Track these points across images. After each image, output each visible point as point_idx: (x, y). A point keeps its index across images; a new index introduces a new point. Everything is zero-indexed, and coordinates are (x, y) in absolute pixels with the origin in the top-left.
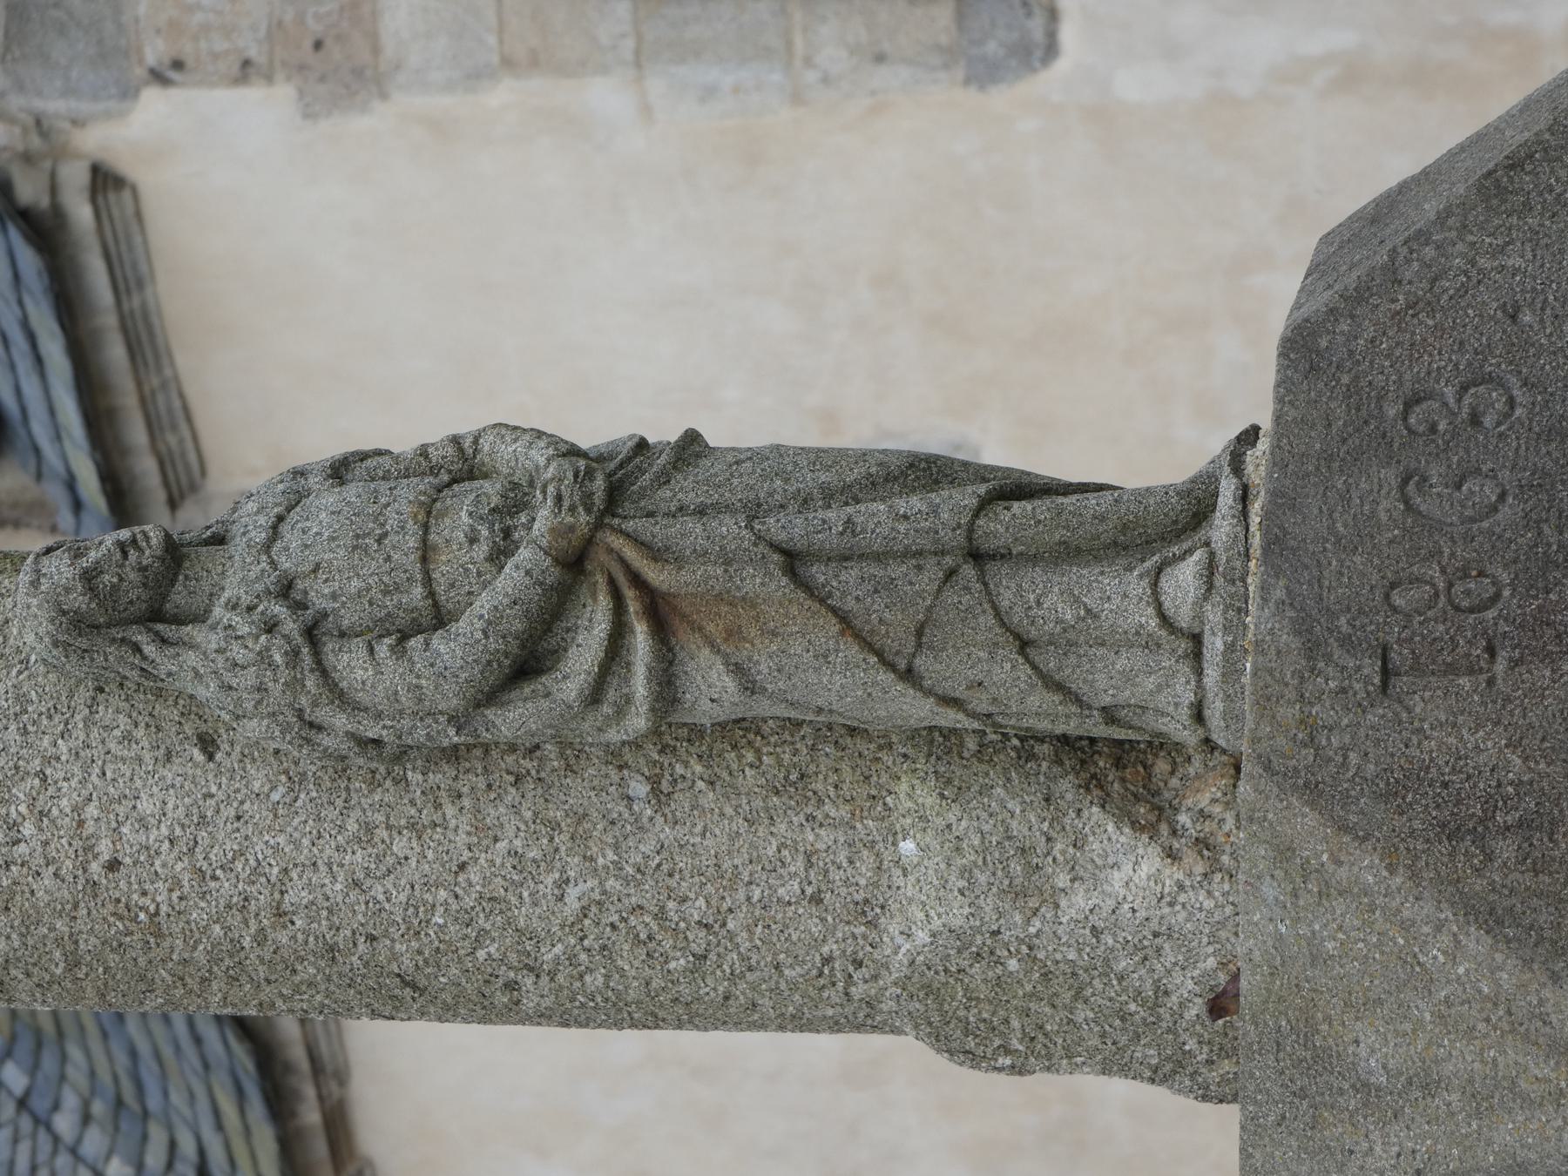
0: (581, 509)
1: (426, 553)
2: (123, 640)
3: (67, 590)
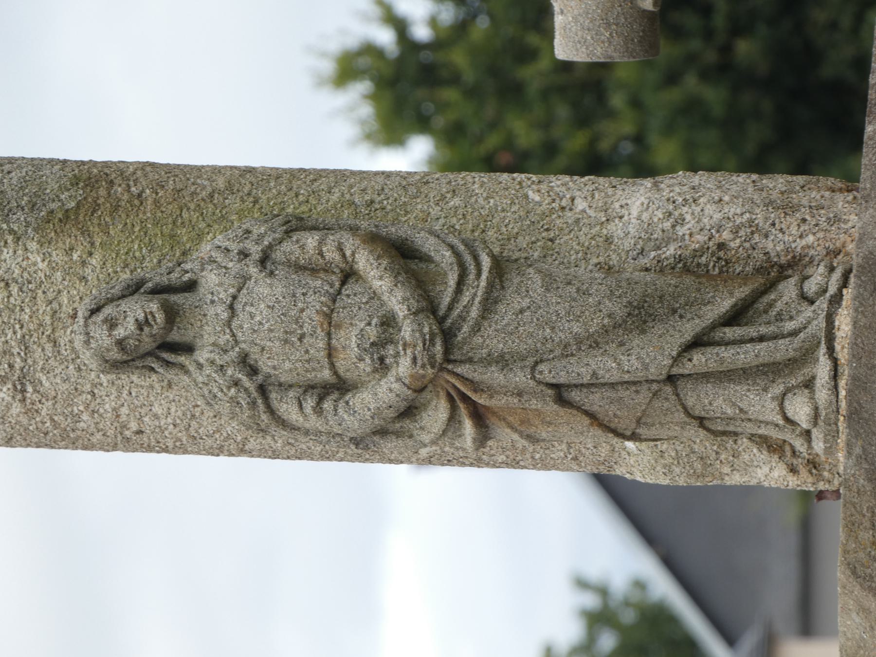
0: (429, 367)
1: (331, 352)
2: (143, 366)
3: (108, 350)
